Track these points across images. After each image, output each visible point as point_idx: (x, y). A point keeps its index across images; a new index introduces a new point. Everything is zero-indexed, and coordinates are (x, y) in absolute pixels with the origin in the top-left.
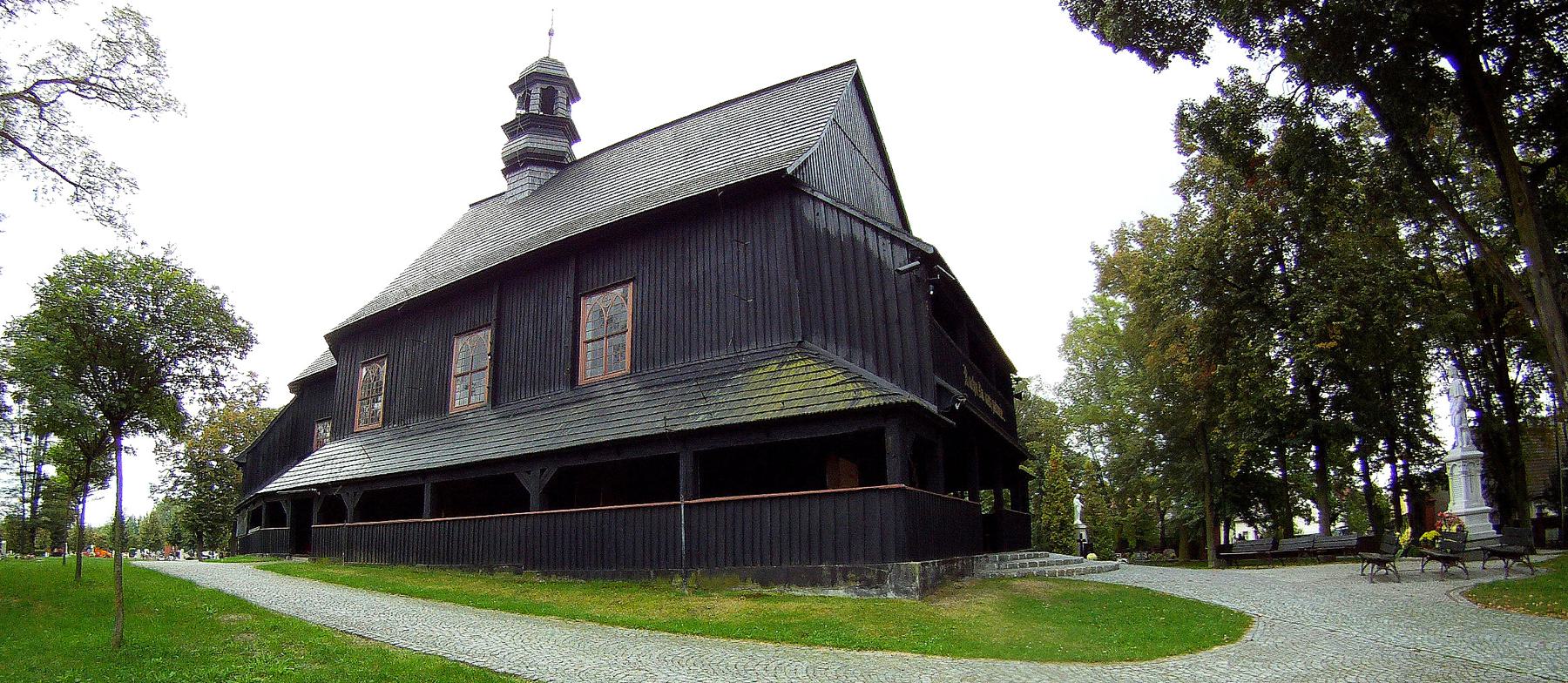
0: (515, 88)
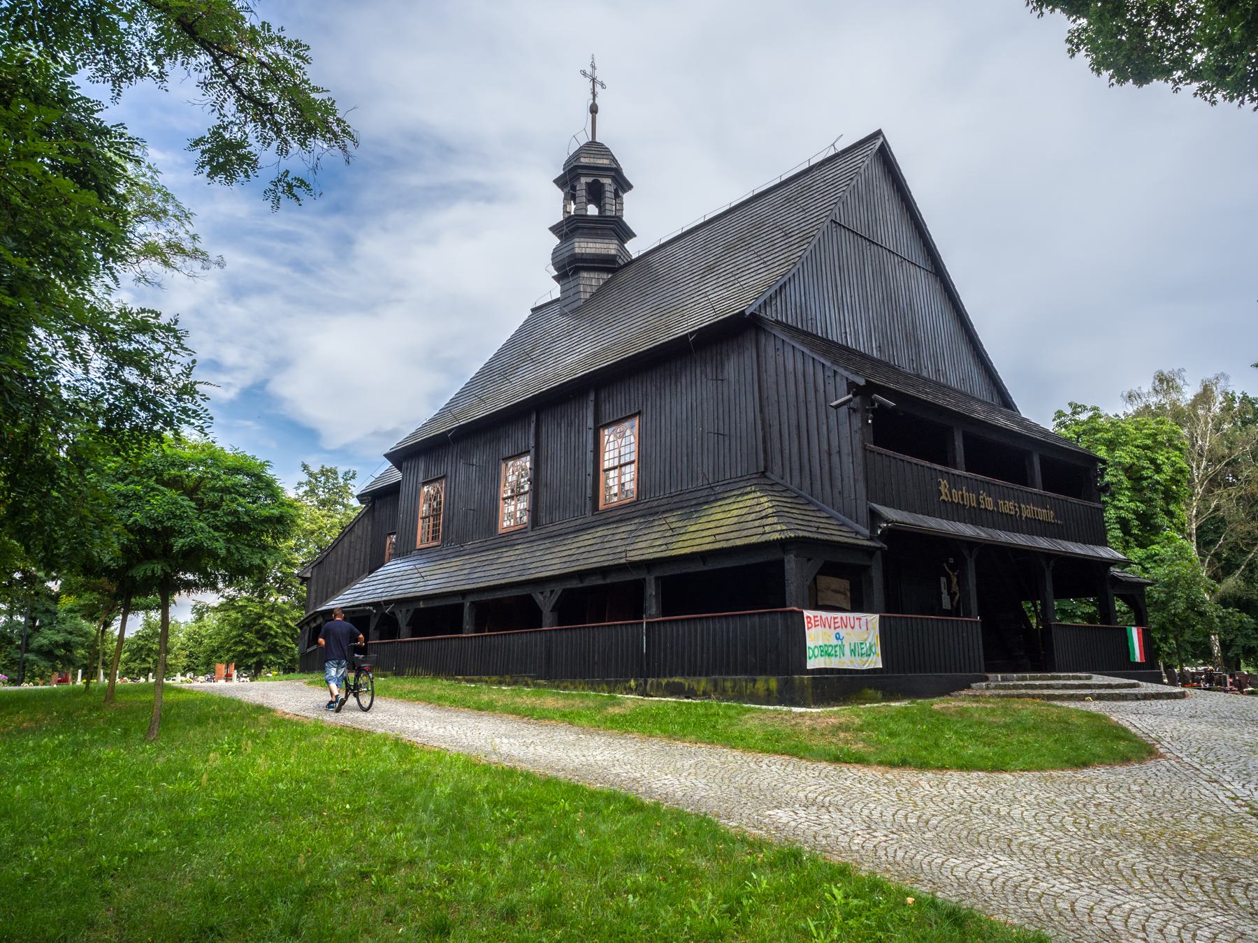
0: (560, 182)
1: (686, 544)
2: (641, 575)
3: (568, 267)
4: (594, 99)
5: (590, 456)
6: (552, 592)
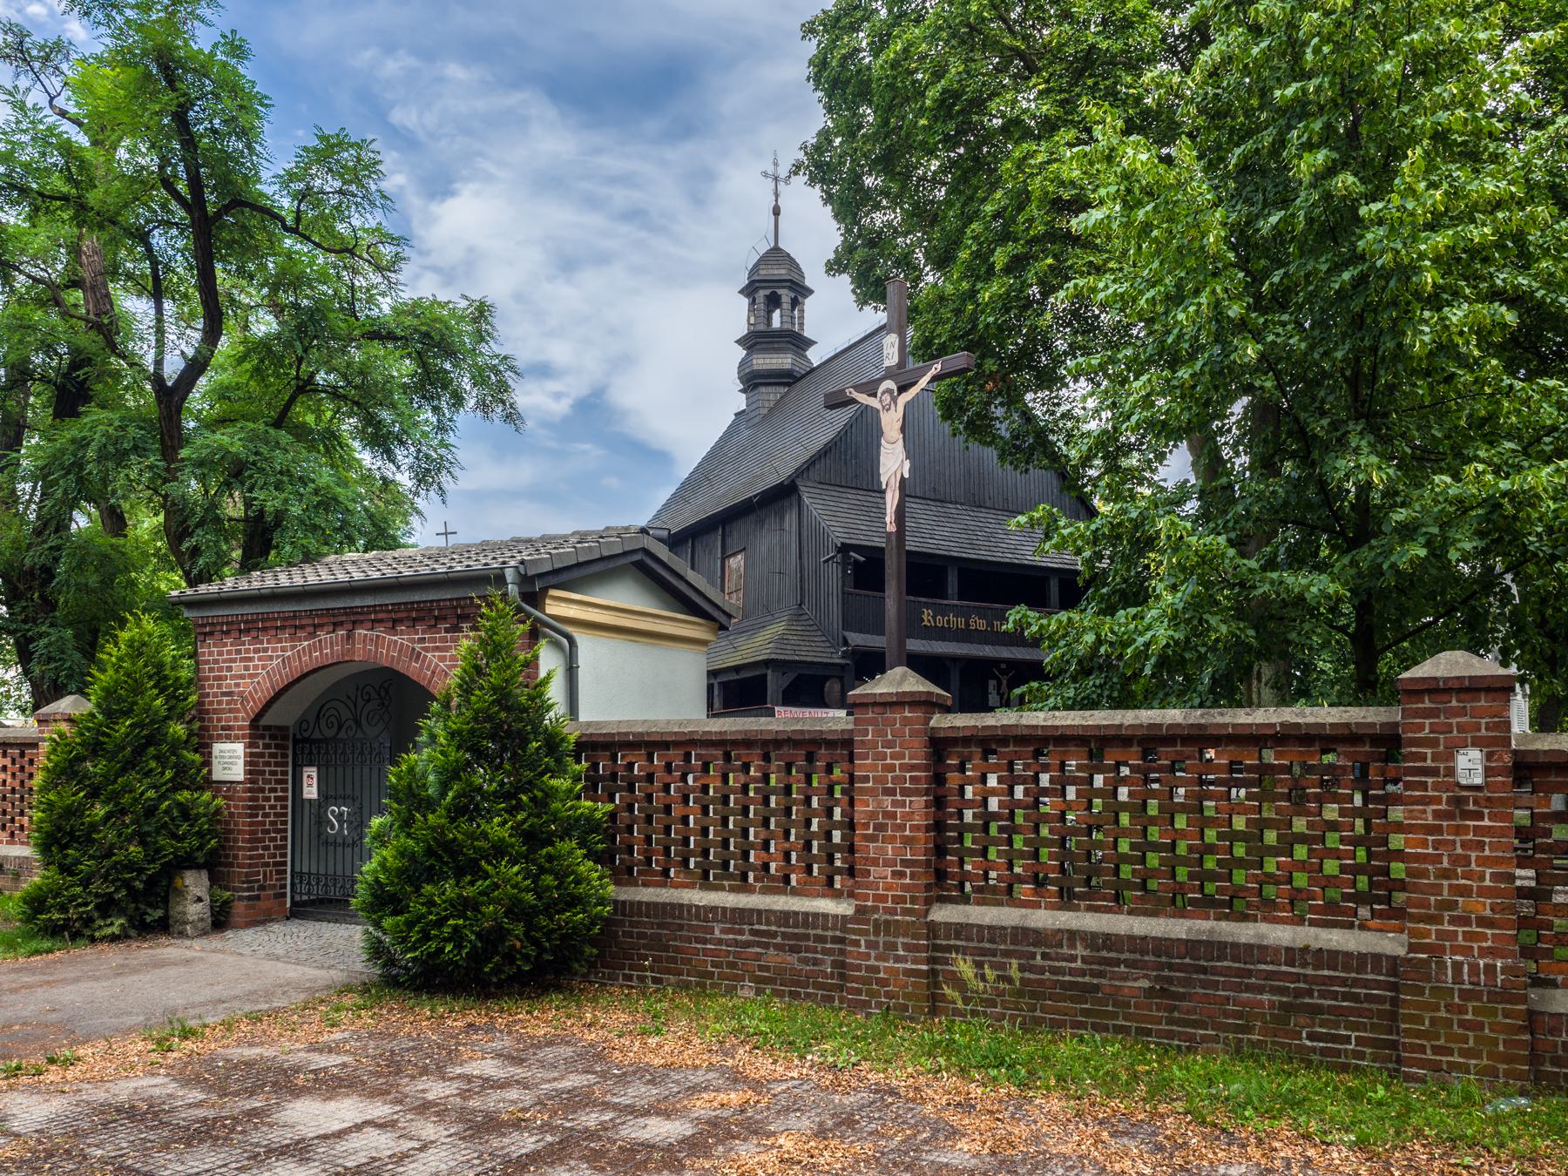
3: (752, 381)
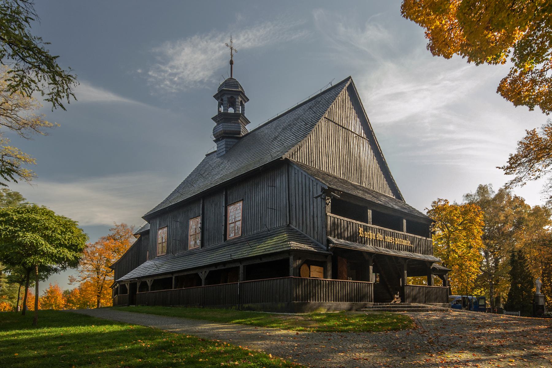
1: (255, 252)
2: (237, 265)
4: (232, 58)
5: (224, 218)
6: (205, 272)
